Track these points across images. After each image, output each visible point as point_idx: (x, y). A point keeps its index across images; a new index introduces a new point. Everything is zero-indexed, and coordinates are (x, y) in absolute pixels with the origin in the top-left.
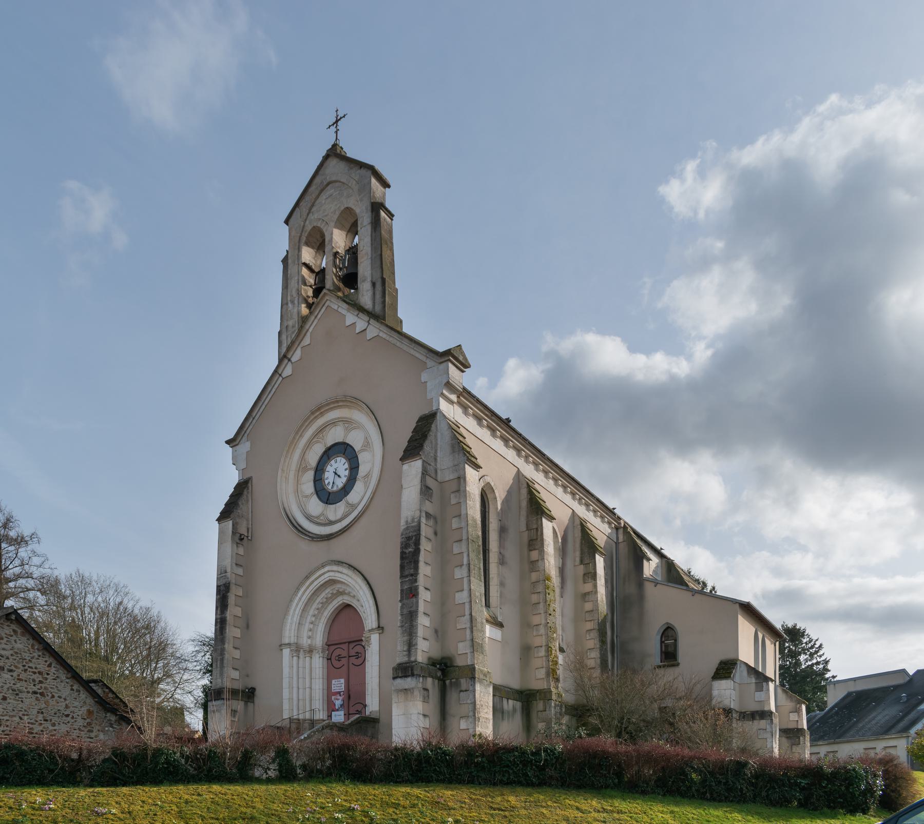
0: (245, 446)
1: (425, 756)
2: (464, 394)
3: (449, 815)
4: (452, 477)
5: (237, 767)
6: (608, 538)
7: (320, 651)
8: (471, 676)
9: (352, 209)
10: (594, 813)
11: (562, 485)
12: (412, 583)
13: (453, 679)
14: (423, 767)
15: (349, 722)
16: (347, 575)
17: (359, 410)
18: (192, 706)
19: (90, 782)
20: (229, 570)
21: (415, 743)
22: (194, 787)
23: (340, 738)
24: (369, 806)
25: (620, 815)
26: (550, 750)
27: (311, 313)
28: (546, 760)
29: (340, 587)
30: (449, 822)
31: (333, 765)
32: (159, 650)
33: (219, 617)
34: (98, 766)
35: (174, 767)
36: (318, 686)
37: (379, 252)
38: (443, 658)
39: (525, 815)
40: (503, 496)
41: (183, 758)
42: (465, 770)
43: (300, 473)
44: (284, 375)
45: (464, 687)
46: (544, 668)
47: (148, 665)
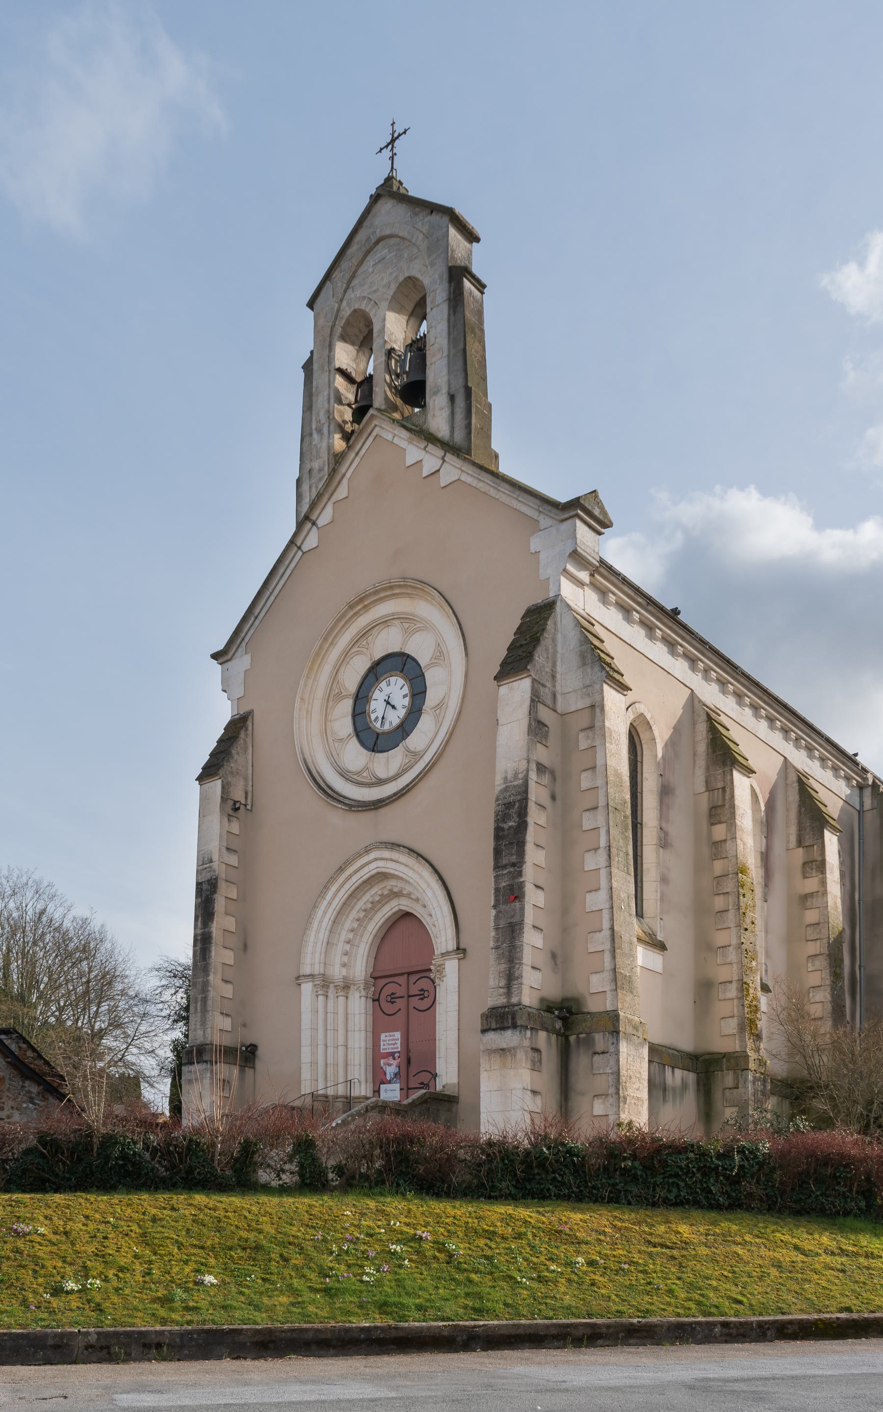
0: (242, 662)
1: (537, 1156)
2: (602, 570)
3: (578, 1252)
4: (580, 705)
5: (232, 1167)
6: (847, 805)
7: (362, 987)
8: (612, 1029)
9: (417, 279)
10: (824, 1256)
11: (766, 716)
12: (514, 878)
13: (582, 1033)
14: (534, 1175)
15: (410, 1100)
16: (406, 865)
17: (427, 600)
18: (155, 1072)
19: (5, 1185)
20: (216, 857)
21: (520, 1135)
22: (165, 1196)
23: (396, 1126)
24: (446, 1234)
25: (871, 1260)
26: (748, 1150)
27: (349, 447)
28: (741, 1167)
29: (395, 884)
30: (578, 1263)
31: (387, 1168)
32: (103, 986)
33: (199, 931)
34: (17, 1160)
35: (134, 1164)
36: (359, 1042)
37: (461, 346)
38: (565, 1000)
39: (707, 1255)
40: (667, 736)
41: (148, 1151)
42: (604, 1181)
43: (330, 704)
44: (305, 548)
45: (600, 1045)
46: (735, 1018)
47: (84, 1009)
